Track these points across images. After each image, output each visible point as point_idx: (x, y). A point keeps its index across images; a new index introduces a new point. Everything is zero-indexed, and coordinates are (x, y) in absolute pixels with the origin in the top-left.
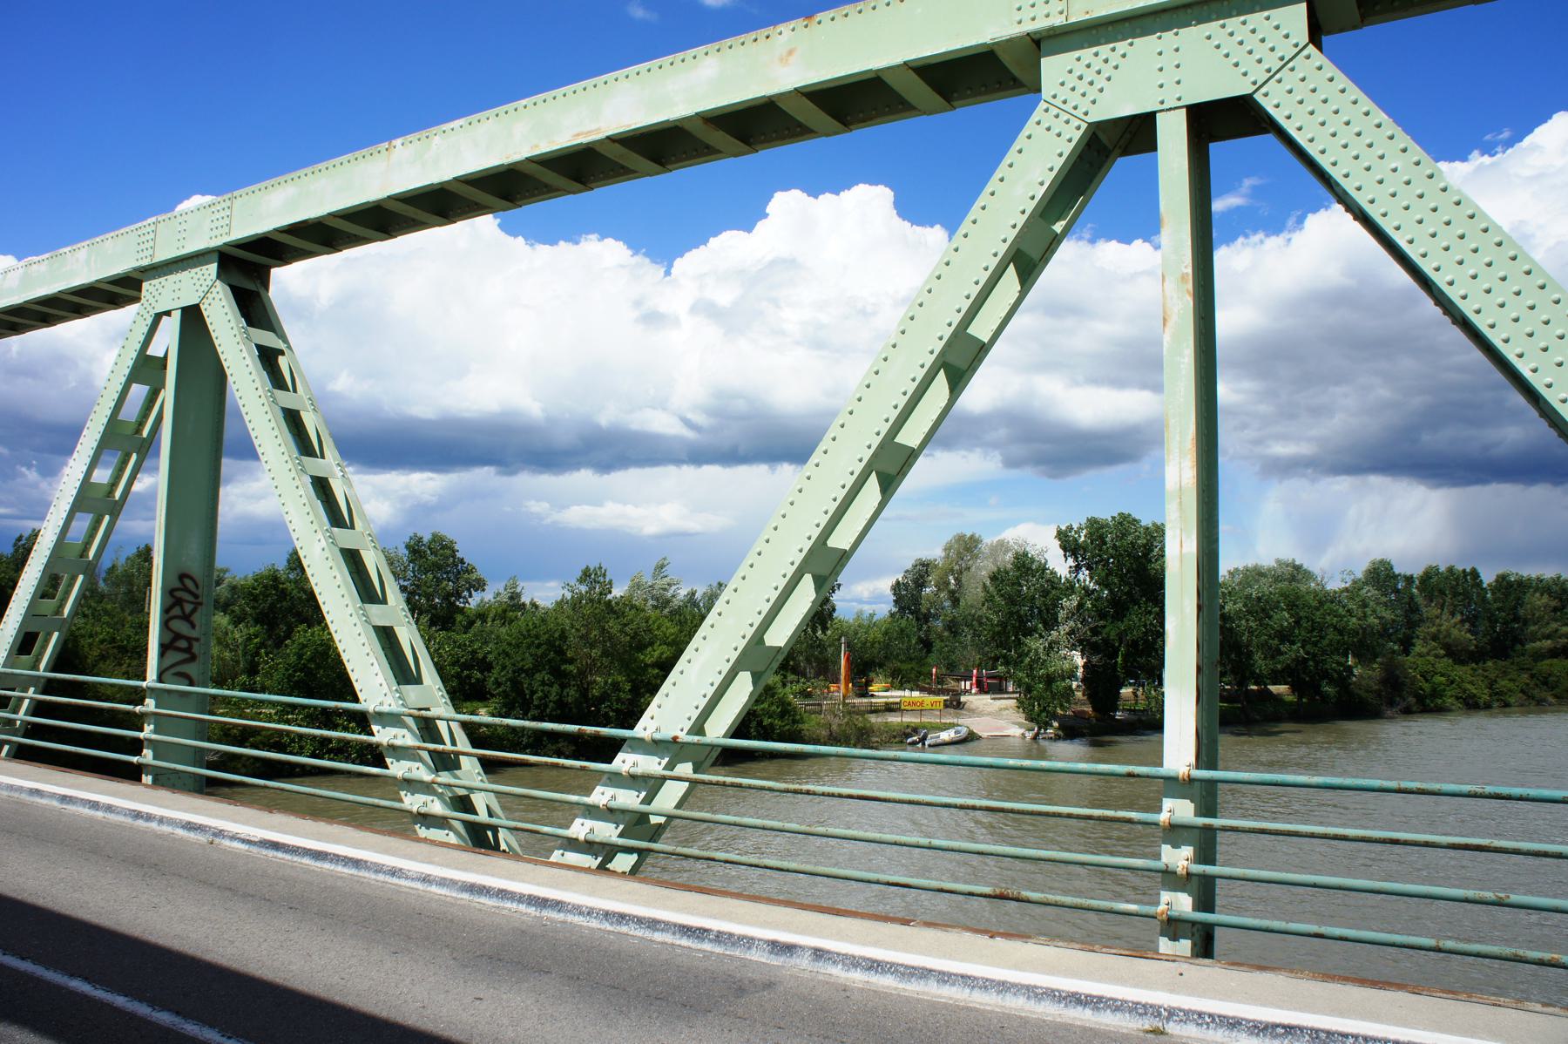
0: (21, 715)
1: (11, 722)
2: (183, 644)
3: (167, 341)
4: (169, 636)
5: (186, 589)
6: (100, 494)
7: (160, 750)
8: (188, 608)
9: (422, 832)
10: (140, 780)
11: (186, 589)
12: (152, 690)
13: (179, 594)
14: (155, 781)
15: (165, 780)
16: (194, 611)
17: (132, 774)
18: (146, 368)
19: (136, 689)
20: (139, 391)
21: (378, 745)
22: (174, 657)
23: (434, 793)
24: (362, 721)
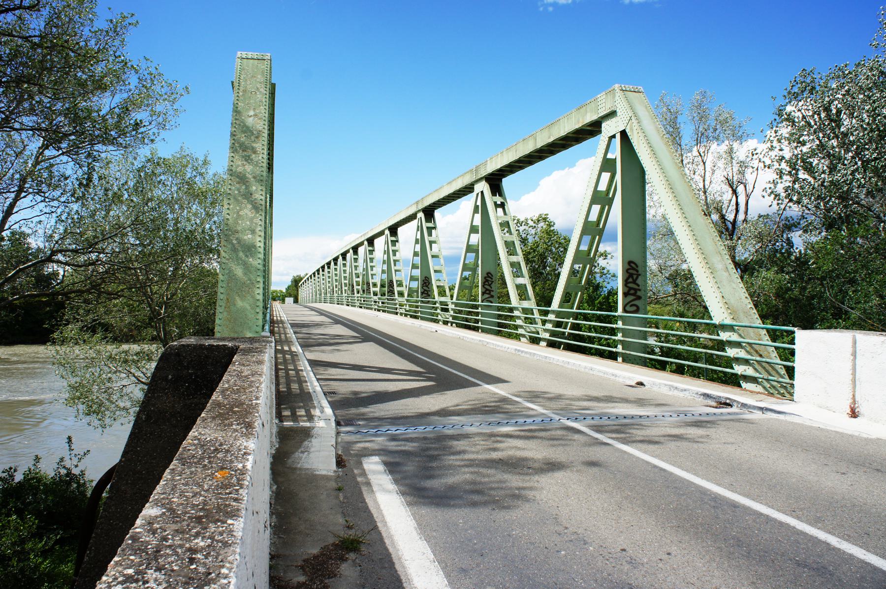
0: (568, 331)
1: (564, 333)
2: (632, 292)
3: (616, 153)
4: (626, 290)
5: (633, 269)
6: (603, 195)
7: (625, 333)
8: (635, 277)
9: (744, 385)
10: (616, 360)
11: (633, 269)
12: (621, 316)
13: (631, 271)
14: (624, 361)
15: (627, 359)
16: (637, 278)
17: (613, 356)
18: (607, 165)
19: (613, 329)
20: (606, 176)
21: (736, 375)
22: (630, 298)
23: (742, 347)
24: (715, 328)
